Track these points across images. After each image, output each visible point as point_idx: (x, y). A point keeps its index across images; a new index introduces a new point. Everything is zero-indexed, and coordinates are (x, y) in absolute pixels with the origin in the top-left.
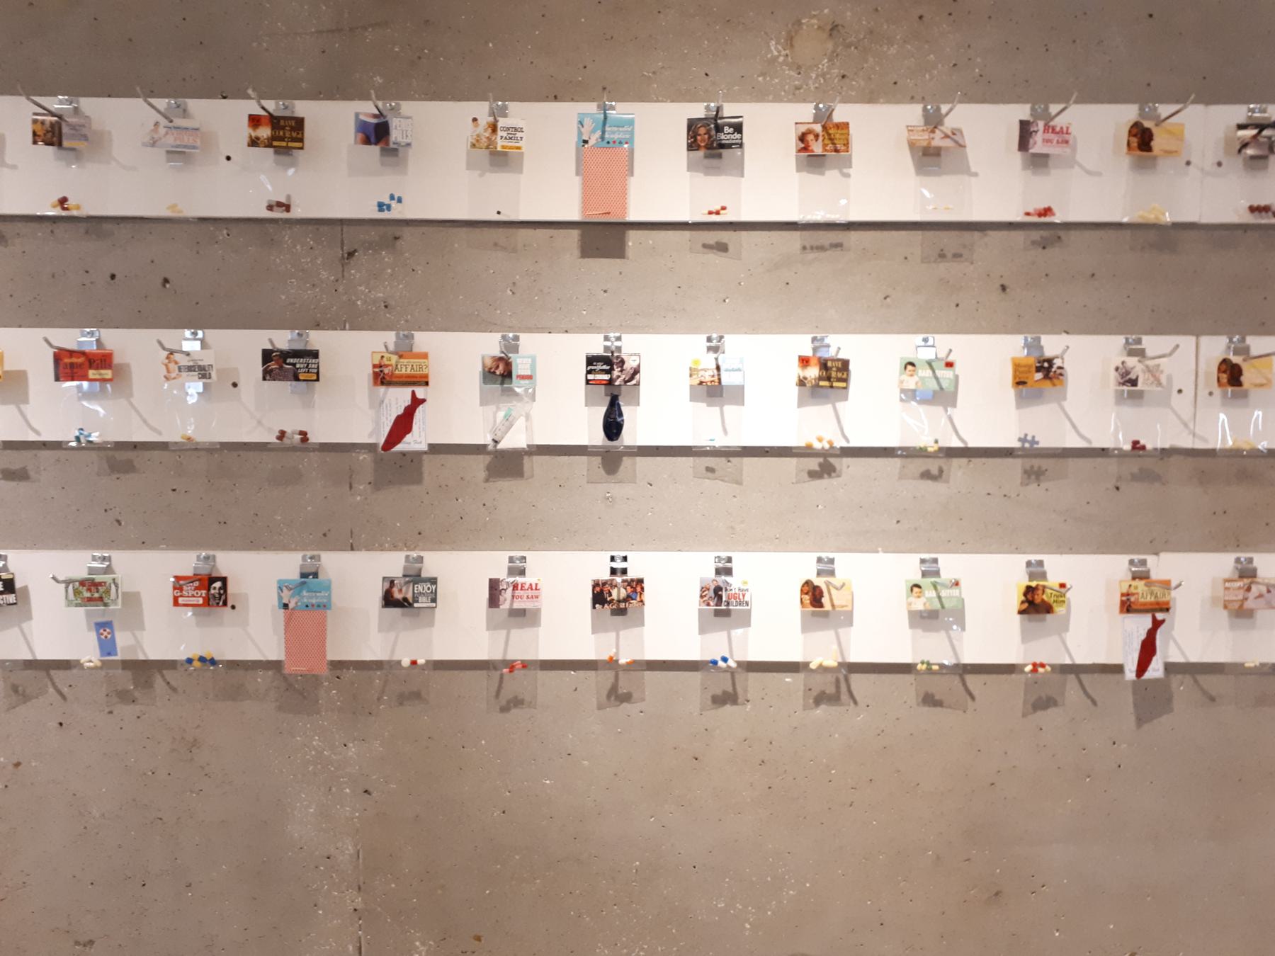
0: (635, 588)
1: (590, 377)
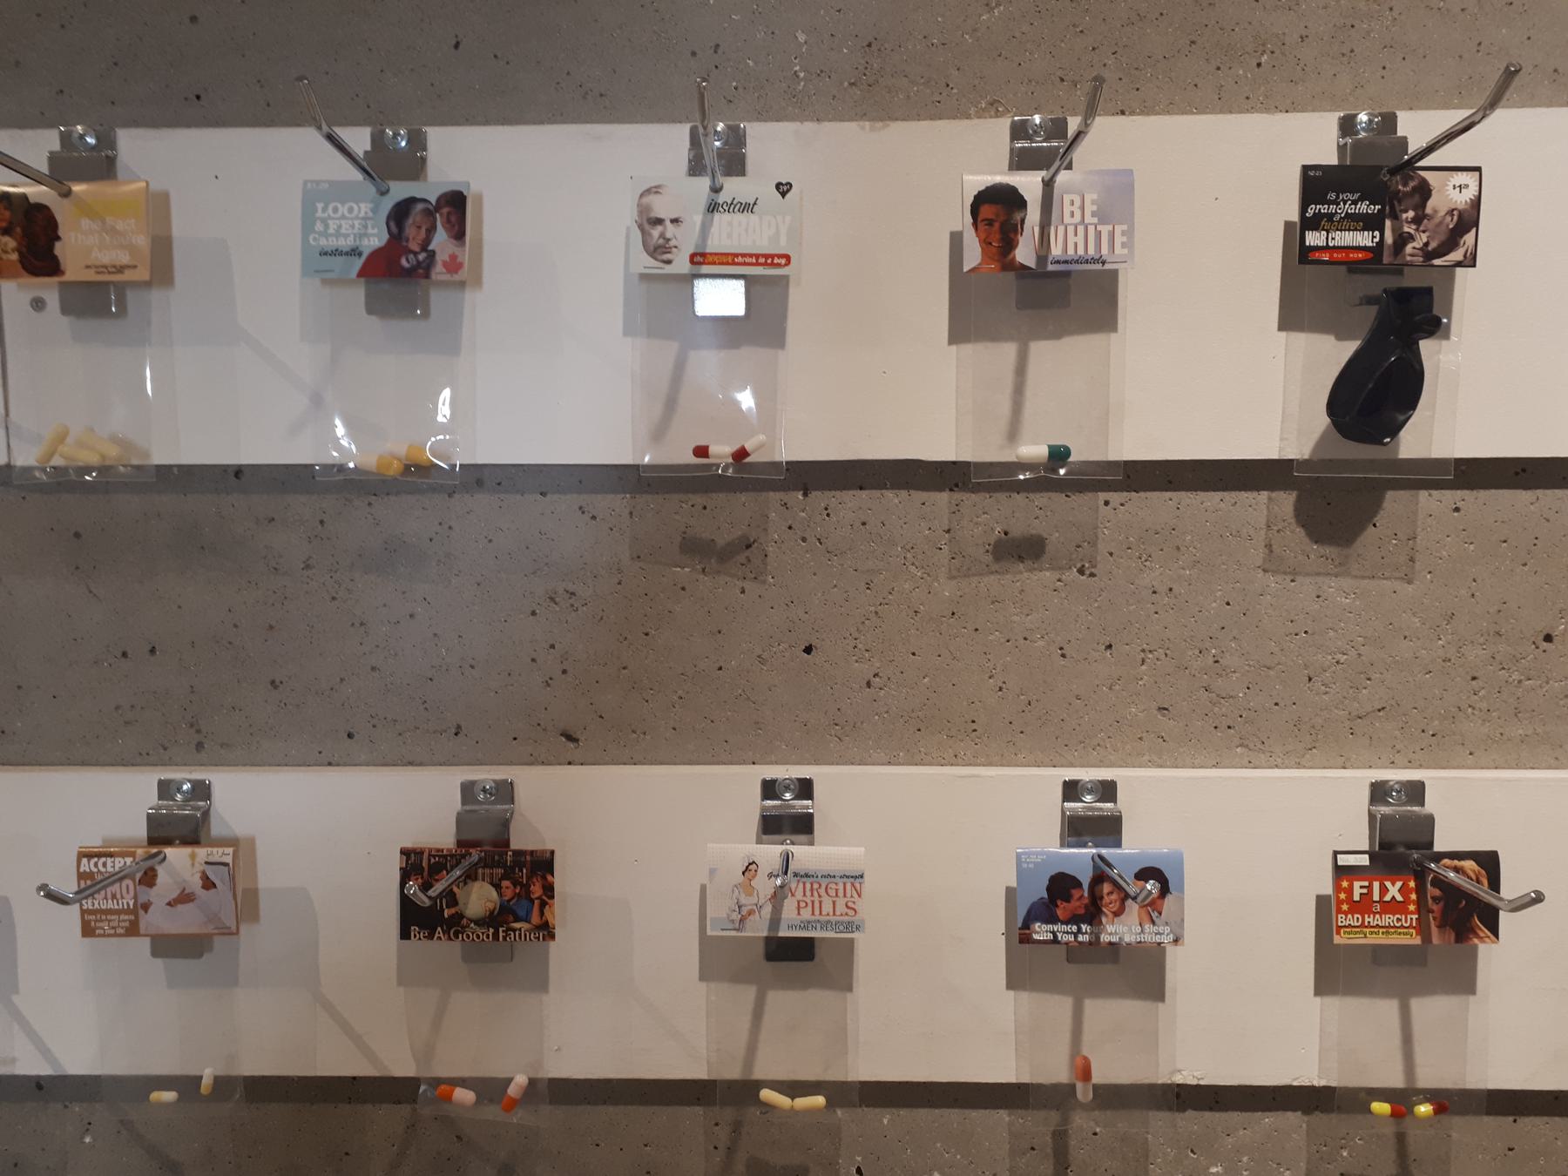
0: (526, 888)
1: (1314, 238)
